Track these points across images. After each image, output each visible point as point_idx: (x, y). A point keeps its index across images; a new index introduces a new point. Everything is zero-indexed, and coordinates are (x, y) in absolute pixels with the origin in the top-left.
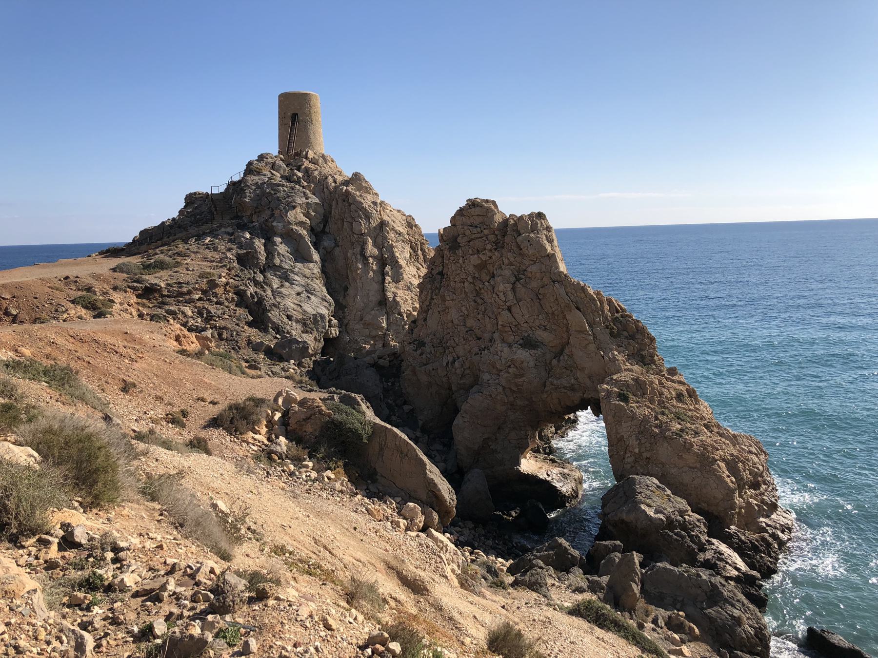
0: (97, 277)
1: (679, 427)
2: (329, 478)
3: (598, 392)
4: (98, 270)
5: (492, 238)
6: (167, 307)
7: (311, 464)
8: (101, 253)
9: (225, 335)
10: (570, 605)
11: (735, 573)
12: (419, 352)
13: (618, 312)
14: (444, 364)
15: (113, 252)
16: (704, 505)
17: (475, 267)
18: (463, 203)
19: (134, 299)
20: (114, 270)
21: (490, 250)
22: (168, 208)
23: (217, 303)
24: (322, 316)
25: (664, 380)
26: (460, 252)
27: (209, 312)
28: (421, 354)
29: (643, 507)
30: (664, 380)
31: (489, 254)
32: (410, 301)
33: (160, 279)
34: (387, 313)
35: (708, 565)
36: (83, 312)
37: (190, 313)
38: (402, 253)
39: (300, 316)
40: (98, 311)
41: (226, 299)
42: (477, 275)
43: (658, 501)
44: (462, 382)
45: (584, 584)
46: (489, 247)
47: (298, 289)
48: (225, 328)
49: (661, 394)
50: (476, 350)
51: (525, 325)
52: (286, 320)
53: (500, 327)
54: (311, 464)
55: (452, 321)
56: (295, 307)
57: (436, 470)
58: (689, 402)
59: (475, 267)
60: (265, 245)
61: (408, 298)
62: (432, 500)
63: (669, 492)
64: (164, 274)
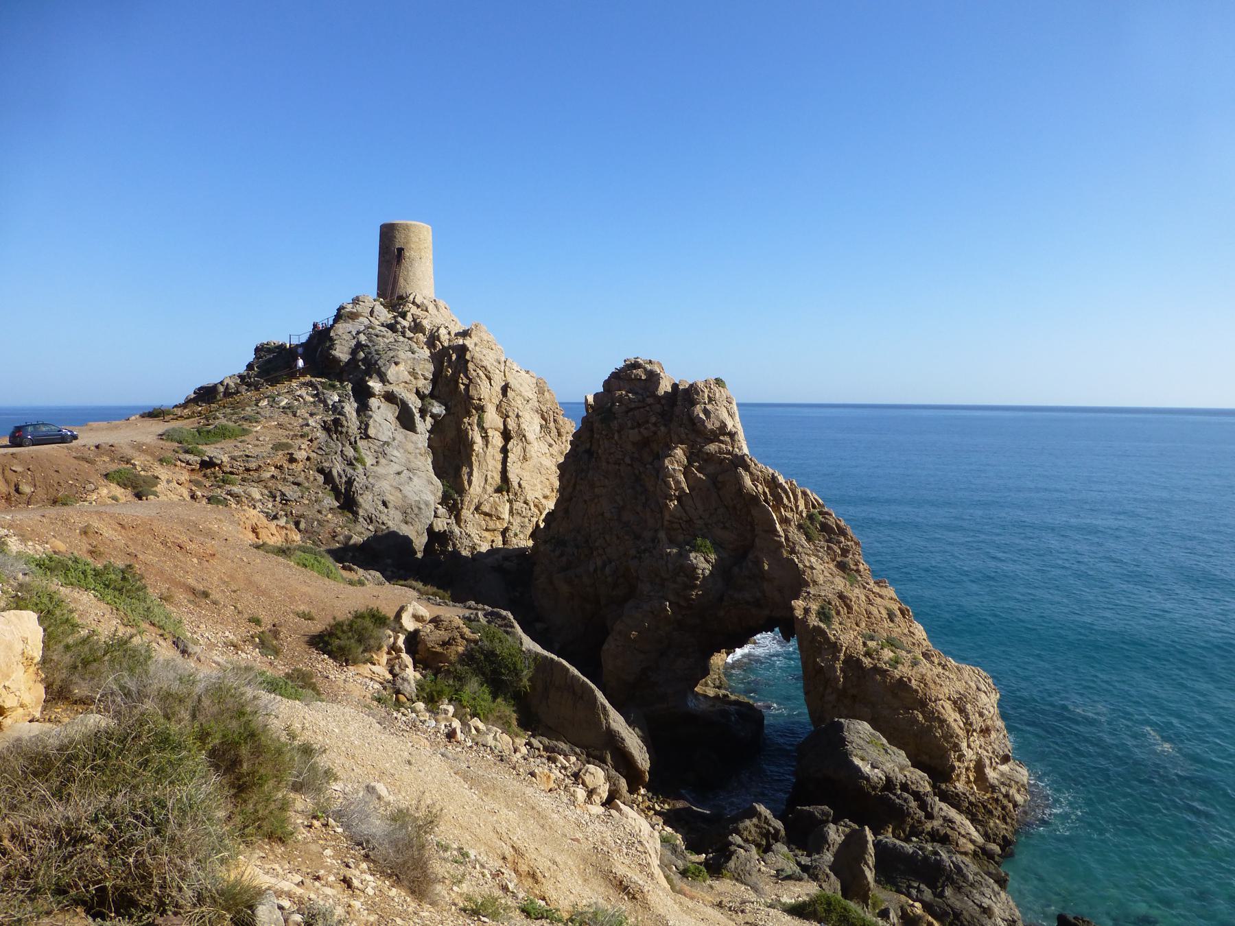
0: (139, 447)
1: (892, 654)
2: (477, 729)
3: (792, 609)
4: (140, 438)
5: (658, 408)
6: (228, 487)
7: (451, 709)
8: (143, 416)
9: (302, 526)
10: (789, 901)
11: (971, 847)
12: (557, 553)
13: (814, 507)
14: (591, 569)
15: (154, 414)
16: (925, 758)
17: (633, 444)
18: (621, 365)
19: (185, 476)
20: (75, 437)
21: (655, 424)
22: (229, 361)
23: (294, 483)
24: (427, 504)
25: (871, 596)
26: (615, 425)
27: (283, 494)
28: (562, 555)
29: (857, 761)
30: (871, 596)
31: (653, 429)
32: (539, 486)
33: (218, 451)
34: (510, 501)
35: (935, 837)
36: (118, 491)
37: (258, 496)
38: (532, 425)
39: (400, 503)
40: (140, 489)
41: (307, 479)
42: (636, 455)
43: (873, 753)
44: (644, 594)
45: (791, 867)
46: (653, 419)
47: (397, 468)
48: (302, 516)
49: (869, 614)
50: (633, 552)
51: (700, 522)
52: (381, 508)
53: (666, 523)
54: (451, 709)
55: (602, 514)
56: (393, 491)
57: (620, 719)
58: (903, 625)
59: (633, 444)
60: (358, 411)
61: (537, 482)
62: (623, 762)
63: (885, 741)
64: (228, 444)
